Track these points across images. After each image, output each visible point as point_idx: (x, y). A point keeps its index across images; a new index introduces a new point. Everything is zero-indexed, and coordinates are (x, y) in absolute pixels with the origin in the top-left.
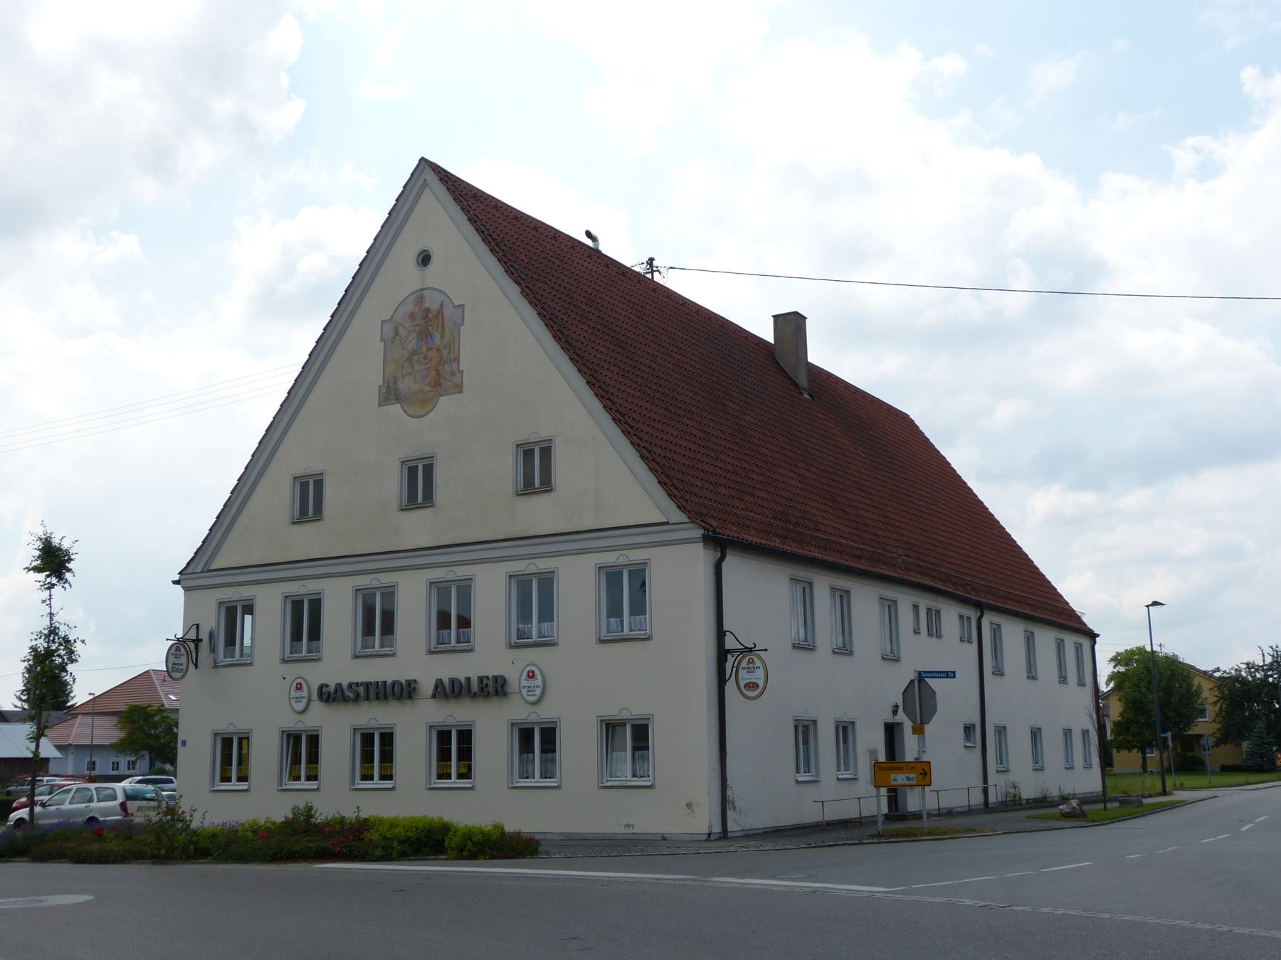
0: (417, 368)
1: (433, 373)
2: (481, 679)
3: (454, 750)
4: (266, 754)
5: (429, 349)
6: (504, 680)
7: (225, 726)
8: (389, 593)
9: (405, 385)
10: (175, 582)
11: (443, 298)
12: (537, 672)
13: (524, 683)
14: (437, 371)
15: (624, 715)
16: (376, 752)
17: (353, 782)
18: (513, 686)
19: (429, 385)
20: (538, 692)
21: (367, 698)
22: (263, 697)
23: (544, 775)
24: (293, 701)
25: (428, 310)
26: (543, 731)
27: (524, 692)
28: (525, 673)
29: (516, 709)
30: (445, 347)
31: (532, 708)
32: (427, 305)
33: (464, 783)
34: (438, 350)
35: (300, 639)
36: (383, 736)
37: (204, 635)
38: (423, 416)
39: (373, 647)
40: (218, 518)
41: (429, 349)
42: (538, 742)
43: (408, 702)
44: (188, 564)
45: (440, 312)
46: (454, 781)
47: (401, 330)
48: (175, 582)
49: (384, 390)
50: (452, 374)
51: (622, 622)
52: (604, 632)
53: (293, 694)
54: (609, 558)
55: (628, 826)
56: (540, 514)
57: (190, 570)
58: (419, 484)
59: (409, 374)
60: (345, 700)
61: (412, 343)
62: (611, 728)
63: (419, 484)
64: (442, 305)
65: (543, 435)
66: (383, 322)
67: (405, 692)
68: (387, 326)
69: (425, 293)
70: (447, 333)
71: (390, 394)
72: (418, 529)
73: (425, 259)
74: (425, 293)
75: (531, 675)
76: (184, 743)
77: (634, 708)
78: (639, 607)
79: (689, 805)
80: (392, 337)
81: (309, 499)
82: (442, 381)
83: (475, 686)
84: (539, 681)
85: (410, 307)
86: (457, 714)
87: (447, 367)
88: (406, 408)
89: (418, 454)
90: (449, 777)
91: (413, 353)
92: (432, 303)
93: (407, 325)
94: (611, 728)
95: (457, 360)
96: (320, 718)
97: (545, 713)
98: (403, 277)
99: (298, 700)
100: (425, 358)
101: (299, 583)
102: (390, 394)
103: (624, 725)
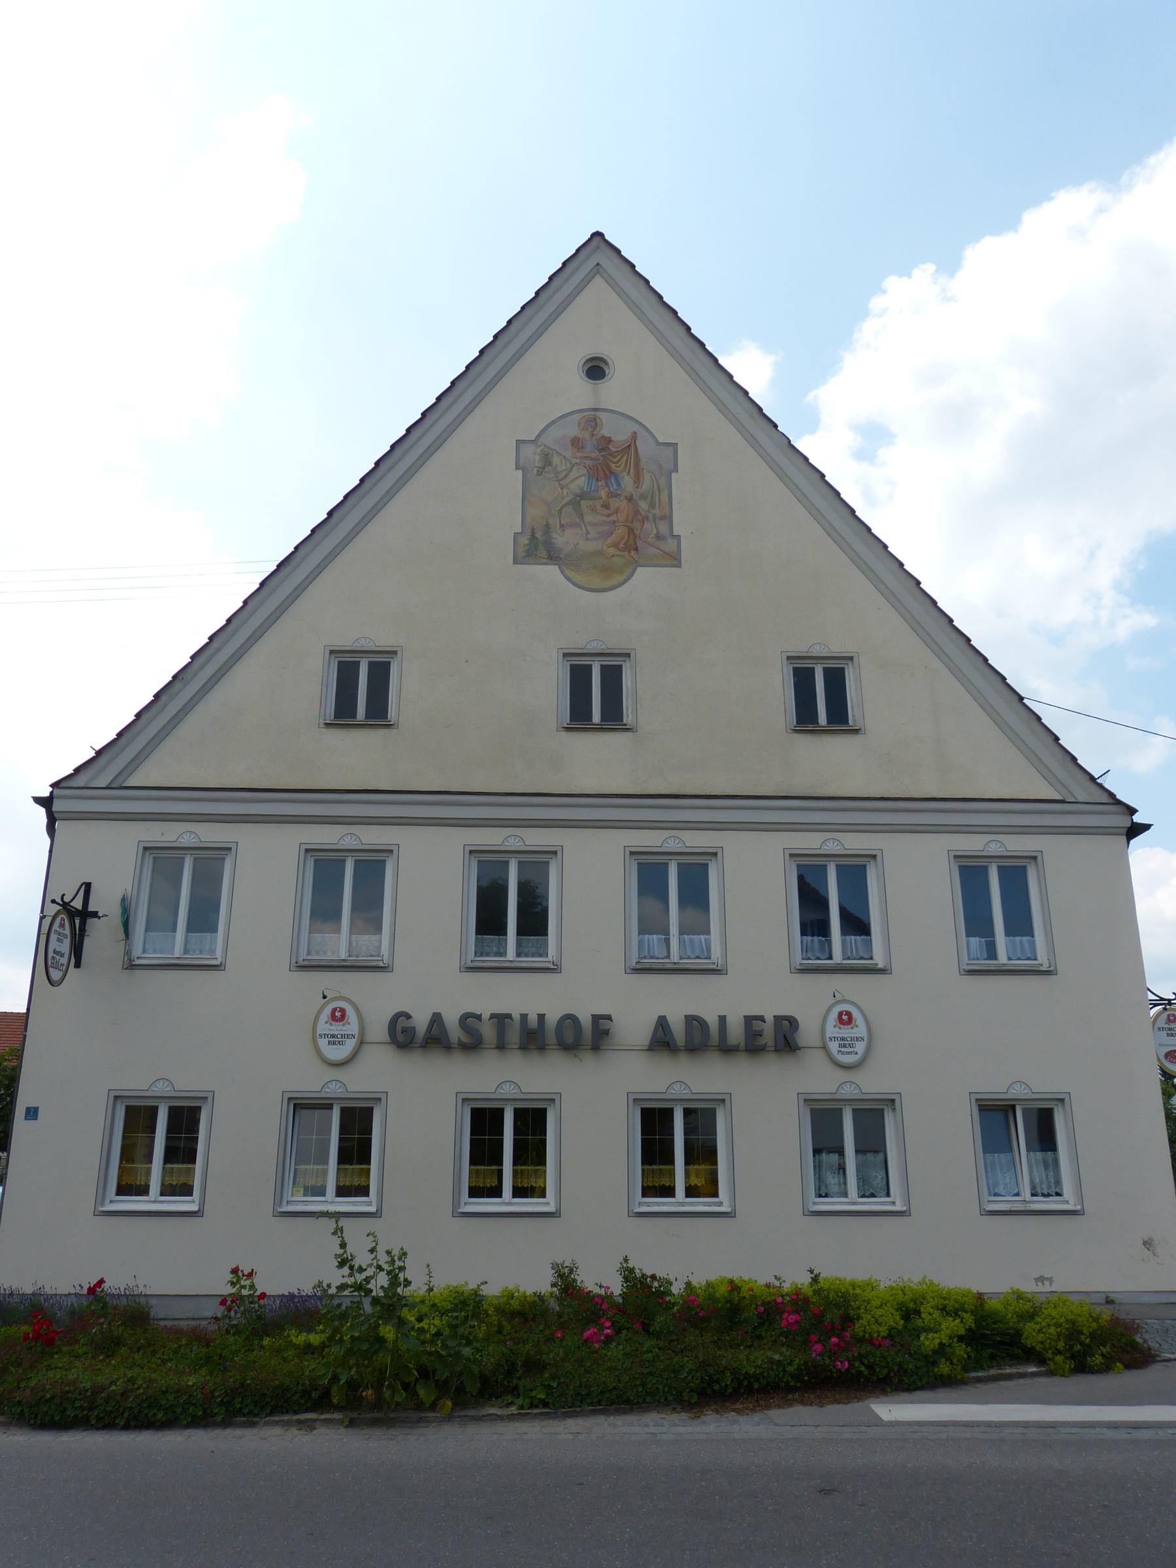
0: (589, 518)
1: (621, 531)
2: (749, 1020)
3: (674, 1148)
4: (241, 1143)
5: (611, 495)
6: (792, 1022)
7: (140, 1081)
8: (536, 866)
9: (564, 540)
10: (38, 800)
11: (636, 428)
12: (856, 1014)
13: (832, 1029)
14: (631, 530)
15: (1018, 1092)
16: (505, 1147)
17: (101, 1197)
18: (807, 1034)
19: (616, 545)
20: (860, 1047)
21: (501, 1046)
22: (247, 1028)
23: (866, 1192)
24: (323, 1043)
25: (609, 440)
26: (519, 1114)
27: (834, 1047)
28: (834, 1015)
29: (817, 1078)
30: (643, 497)
31: (843, 1076)
32: (605, 432)
33: (700, 1204)
34: (630, 499)
35: (501, 930)
36: (176, 1114)
37: (105, 902)
38: (605, 590)
39: (504, 954)
40: (157, 696)
41: (611, 495)
42: (849, 1138)
43: (588, 1058)
44: (77, 770)
45: (630, 447)
46: (507, 1202)
47: (556, 460)
48: (38, 800)
49: (524, 540)
50: (659, 537)
51: (667, 941)
52: (471, 955)
53: (324, 1027)
54: (974, 844)
55: (1041, 1279)
56: (827, 763)
57: (81, 781)
58: (596, 694)
59: (572, 525)
60: (726, 1050)
61: (579, 481)
62: (995, 1115)
63: (596, 694)
64: (634, 436)
65: (613, 643)
66: (519, 442)
67: (585, 1038)
68: (528, 450)
69: (601, 415)
70: (647, 478)
71: (536, 547)
72: (597, 762)
73: (596, 370)
74: (601, 415)
75: (846, 1019)
76: (32, 1113)
77: (1027, 1081)
78: (1020, 924)
79: (1148, 1244)
80: (537, 463)
81: (361, 690)
82: (639, 543)
83: (736, 1033)
84: (860, 1030)
85: (572, 429)
86: (680, 1081)
87: (647, 525)
88: (567, 572)
89: (594, 647)
90: (321, 1191)
91: (582, 496)
92: (619, 433)
93: (568, 454)
94: (995, 1115)
95: (668, 518)
96: (378, 1074)
97: (871, 1084)
98: (551, 389)
99: (334, 1040)
100: (606, 506)
101: (181, 827)
102: (536, 547)
103: (329, 1107)
